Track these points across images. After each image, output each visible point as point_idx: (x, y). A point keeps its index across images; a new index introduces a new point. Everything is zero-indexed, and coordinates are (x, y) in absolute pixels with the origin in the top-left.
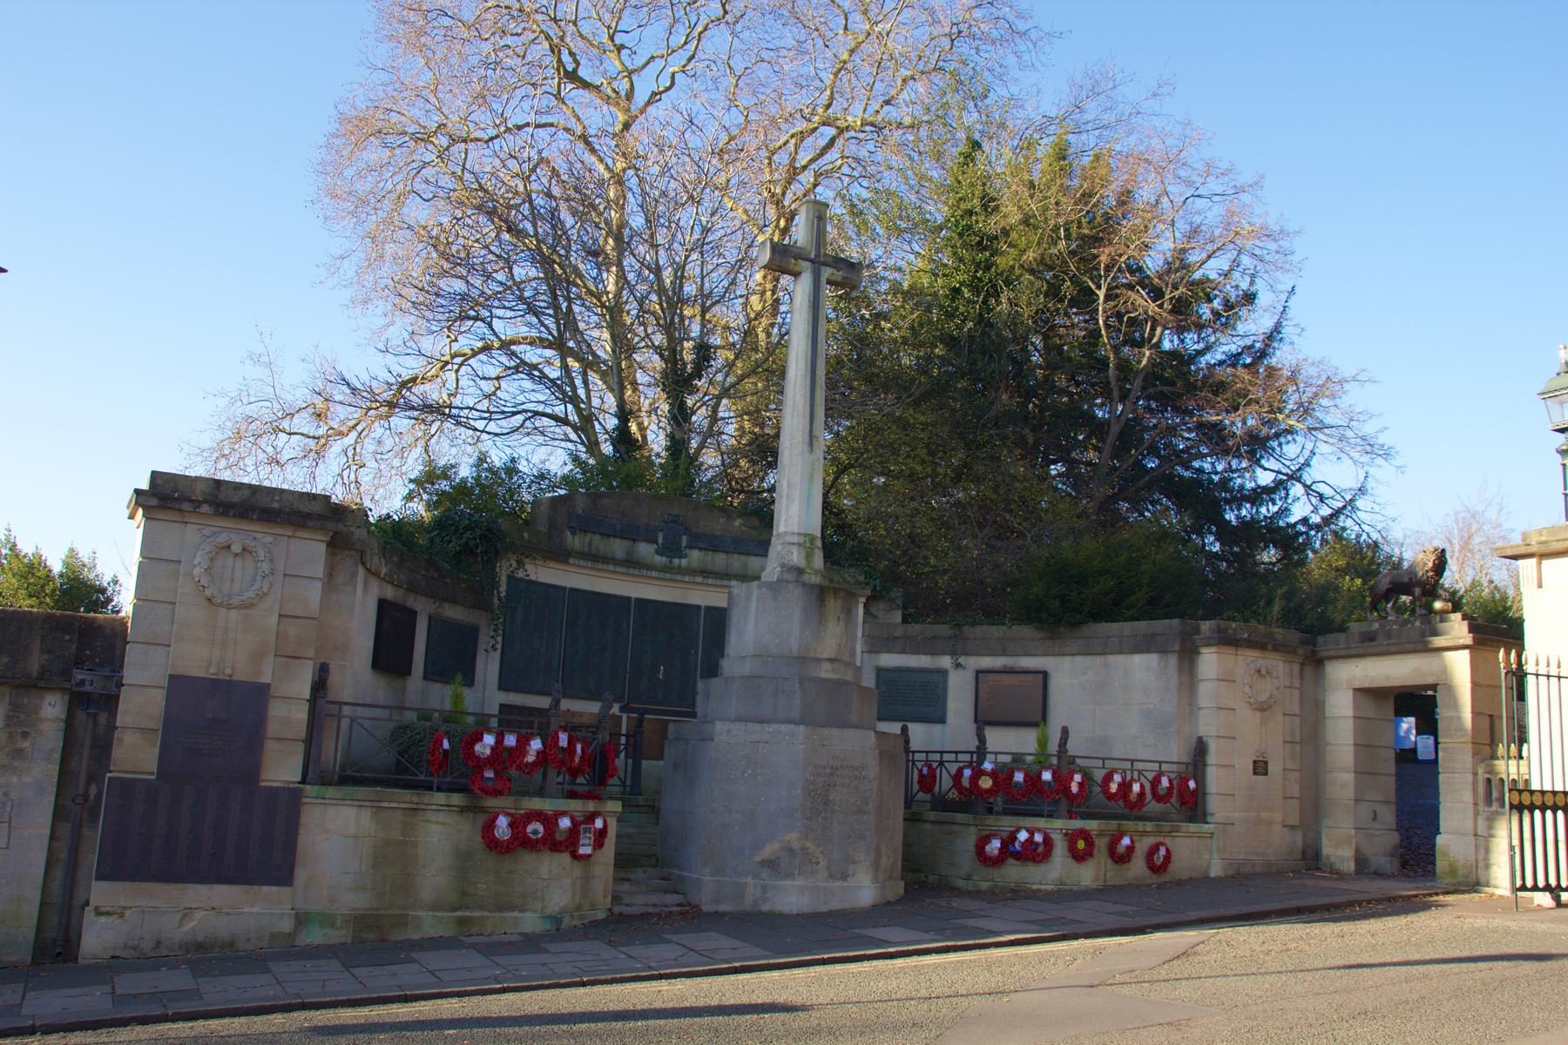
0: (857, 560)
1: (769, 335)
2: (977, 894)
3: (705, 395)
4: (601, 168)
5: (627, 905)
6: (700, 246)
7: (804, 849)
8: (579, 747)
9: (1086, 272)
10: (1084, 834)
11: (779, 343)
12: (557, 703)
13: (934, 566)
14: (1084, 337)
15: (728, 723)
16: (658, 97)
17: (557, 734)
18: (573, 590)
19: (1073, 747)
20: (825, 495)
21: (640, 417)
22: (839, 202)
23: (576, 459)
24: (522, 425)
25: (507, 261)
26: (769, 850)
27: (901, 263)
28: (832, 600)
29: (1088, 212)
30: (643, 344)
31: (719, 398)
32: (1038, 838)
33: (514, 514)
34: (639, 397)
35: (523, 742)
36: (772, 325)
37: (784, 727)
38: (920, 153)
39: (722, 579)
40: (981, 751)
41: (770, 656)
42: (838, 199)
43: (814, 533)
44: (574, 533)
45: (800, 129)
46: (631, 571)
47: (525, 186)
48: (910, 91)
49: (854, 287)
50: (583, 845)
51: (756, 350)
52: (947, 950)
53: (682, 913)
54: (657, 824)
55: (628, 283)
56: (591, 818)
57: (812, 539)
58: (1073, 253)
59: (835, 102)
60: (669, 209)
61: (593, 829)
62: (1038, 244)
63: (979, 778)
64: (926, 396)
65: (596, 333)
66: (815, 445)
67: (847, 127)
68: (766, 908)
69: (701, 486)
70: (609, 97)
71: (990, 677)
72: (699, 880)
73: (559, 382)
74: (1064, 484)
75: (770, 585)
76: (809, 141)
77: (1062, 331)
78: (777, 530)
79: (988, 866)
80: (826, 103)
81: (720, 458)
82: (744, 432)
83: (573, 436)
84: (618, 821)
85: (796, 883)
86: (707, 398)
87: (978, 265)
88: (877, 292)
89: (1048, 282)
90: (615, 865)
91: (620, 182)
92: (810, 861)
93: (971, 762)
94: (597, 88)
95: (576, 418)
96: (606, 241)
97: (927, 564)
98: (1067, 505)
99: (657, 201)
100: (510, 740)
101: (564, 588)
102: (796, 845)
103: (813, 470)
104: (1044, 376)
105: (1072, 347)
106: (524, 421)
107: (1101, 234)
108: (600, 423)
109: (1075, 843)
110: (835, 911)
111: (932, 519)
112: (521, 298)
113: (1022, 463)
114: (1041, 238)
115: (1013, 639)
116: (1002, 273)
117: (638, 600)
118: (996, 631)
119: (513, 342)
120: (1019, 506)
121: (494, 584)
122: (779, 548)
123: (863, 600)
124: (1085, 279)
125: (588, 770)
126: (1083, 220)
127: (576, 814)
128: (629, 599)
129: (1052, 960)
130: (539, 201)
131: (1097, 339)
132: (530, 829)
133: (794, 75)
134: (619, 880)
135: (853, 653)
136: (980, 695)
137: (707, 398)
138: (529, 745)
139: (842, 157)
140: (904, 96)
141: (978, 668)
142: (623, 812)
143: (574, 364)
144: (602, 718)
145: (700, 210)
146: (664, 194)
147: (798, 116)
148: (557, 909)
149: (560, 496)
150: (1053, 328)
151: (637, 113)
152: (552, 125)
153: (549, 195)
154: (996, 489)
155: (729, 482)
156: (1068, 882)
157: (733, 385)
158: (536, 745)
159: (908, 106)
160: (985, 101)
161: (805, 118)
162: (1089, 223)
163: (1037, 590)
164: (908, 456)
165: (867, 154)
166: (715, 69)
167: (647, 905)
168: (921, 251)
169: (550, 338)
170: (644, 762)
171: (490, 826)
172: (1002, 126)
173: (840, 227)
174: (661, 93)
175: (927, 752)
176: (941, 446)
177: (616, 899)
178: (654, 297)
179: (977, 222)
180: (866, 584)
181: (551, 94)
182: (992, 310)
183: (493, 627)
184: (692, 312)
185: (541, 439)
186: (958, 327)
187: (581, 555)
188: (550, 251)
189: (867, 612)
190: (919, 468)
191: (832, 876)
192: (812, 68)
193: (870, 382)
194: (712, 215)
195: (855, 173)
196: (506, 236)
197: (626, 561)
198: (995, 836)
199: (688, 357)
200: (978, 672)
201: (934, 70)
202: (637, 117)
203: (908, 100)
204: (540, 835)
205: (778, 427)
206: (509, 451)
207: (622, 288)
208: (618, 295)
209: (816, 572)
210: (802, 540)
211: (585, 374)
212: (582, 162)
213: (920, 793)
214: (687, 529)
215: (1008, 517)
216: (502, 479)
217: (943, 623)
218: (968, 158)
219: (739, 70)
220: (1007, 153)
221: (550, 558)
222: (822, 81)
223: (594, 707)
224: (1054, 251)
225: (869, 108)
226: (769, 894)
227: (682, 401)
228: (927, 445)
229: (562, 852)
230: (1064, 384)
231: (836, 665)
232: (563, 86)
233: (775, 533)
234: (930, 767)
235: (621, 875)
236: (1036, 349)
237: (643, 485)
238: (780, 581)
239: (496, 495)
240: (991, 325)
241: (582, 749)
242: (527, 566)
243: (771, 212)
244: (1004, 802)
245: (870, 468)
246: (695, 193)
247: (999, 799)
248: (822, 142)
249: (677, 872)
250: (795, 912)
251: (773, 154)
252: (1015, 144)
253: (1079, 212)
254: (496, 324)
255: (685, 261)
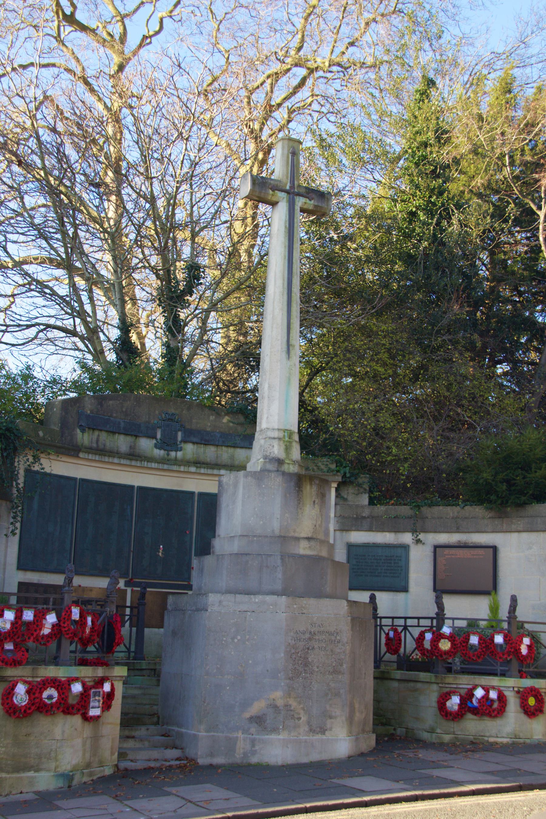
0: (330, 450)
1: (250, 255)
2: (440, 746)
3: (196, 309)
4: (101, 107)
5: (132, 761)
6: (189, 178)
7: (287, 706)
8: (89, 619)
9: (528, 194)
10: (534, 692)
11: (259, 263)
12: (69, 581)
13: (396, 456)
14: (526, 253)
15: (219, 595)
16: (148, 41)
17: (70, 609)
18: (83, 481)
19: (521, 614)
20: (301, 394)
21: (138, 327)
22: (309, 136)
23: (84, 366)
24: (36, 337)
25: (19, 190)
26: (256, 708)
27: (366, 193)
28: (308, 487)
29: (530, 141)
30: (140, 265)
31: (207, 312)
32: (493, 695)
33: (29, 414)
34: (138, 310)
35: (40, 617)
36: (253, 246)
37: (269, 599)
38: (381, 91)
39: (213, 468)
40: (440, 617)
41: (255, 536)
42: (309, 134)
43: (292, 429)
44: (83, 431)
45: (275, 71)
46: (134, 463)
47: (33, 124)
48: (372, 33)
49: (324, 215)
50: (93, 708)
51: (238, 268)
52: (415, 799)
53: (180, 767)
54: (158, 685)
55: (127, 212)
56: (100, 682)
57: (291, 434)
58: (517, 178)
59: (305, 44)
60: (161, 145)
61: (101, 693)
62: (486, 170)
63: (439, 641)
64: (388, 306)
65: (99, 255)
66: (292, 352)
67: (317, 68)
68: (254, 760)
69: (193, 389)
70: (105, 40)
71: (447, 551)
72: (195, 735)
73: (68, 299)
74: (509, 381)
75: (254, 474)
76: (283, 81)
77: (507, 248)
78: (260, 426)
79: (449, 719)
80: (297, 45)
81: (209, 362)
82: (229, 341)
83: (81, 345)
84: (124, 684)
85: (281, 737)
86: (197, 312)
87: (432, 191)
88: (344, 216)
89: (494, 205)
90: (121, 724)
91: (118, 120)
92: (293, 717)
93: (432, 627)
94: (93, 31)
95: (83, 328)
96: (106, 174)
97: (390, 454)
98: (512, 400)
99: (151, 139)
100: (28, 615)
101: (74, 479)
102: (280, 703)
103: (290, 374)
104: (490, 287)
105: (515, 262)
106: (38, 333)
107: (542, 161)
108: (104, 334)
109: (527, 700)
110: (315, 762)
111: (394, 414)
112: (32, 224)
113: (471, 363)
114: (488, 165)
115: (466, 518)
116: (453, 197)
117: (140, 488)
118: (451, 511)
119: (25, 262)
120: (469, 402)
121: (14, 477)
122: (262, 442)
123: (335, 485)
124: (527, 201)
125: (98, 639)
126: (526, 148)
127: (87, 680)
128: (133, 487)
129: (511, 810)
130: (46, 136)
131: (538, 254)
132: (45, 694)
133: (269, 19)
134: (124, 738)
135: (327, 533)
136: (438, 567)
137: (197, 312)
138: (45, 619)
139: (312, 95)
140: (367, 38)
141: (436, 543)
142: (128, 676)
143: (80, 282)
144: (109, 593)
145: (188, 145)
146: (156, 131)
147: (273, 58)
148: (69, 767)
149: (72, 399)
150: (497, 246)
151: (130, 55)
152: (54, 65)
153: (54, 130)
154: (449, 388)
155: (218, 384)
156: (521, 735)
157: (220, 300)
158: (51, 618)
159: (370, 47)
160: (440, 41)
161: (279, 60)
162: (531, 150)
163: (486, 475)
164: (372, 360)
165: (334, 93)
166: (199, 14)
167: (149, 760)
168: (381, 179)
169: (59, 258)
170: (147, 630)
171: (9, 693)
172: (455, 63)
173: (311, 159)
174: (151, 37)
175: (393, 618)
176: (401, 350)
177: (122, 755)
178: (149, 223)
179: (431, 153)
180: (338, 471)
181: (52, 36)
182: (444, 230)
183: (12, 515)
184: (183, 236)
185: (52, 348)
186: (414, 246)
187: (90, 450)
188: (57, 182)
189: (338, 496)
190: (381, 370)
191: (312, 731)
192: (285, 14)
193: (339, 296)
194: (199, 150)
195: (324, 110)
196: (16, 168)
197: (130, 455)
198: (454, 693)
199: (180, 276)
200: (436, 547)
201: (394, 12)
202: (130, 59)
203: (370, 42)
204: (54, 700)
205: (259, 335)
206: (24, 360)
207: (121, 216)
208: (118, 223)
209: (294, 462)
210: (281, 435)
211: (90, 291)
212: (83, 102)
213: (388, 655)
214: (182, 426)
215: (459, 410)
216: (19, 384)
217: (405, 505)
218: (424, 95)
219: (220, 16)
220: (459, 89)
221: (63, 454)
222: (294, 25)
223: (103, 583)
224: (499, 176)
225: (336, 49)
226: (257, 748)
227: (176, 314)
228: (389, 351)
229: (74, 714)
230: (508, 293)
231: (313, 543)
232: (62, 28)
233: (258, 429)
234: (395, 631)
235: (127, 733)
236: (483, 264)
237: (143, 388)
238: (263, 470)
239: (13, 399)
240: (443, 244)
241: (92, 621)
242: (43, 461)
243: (251, 146)
244: (462, 662)
245: (340, 370)
246: (183, 131)
247: (457, 660)
248: (295, 82)
249: (176, 729)
250: (280, 763)
251: (251, 94)
252: (466, 80)
253: (523, 141)
254: (10, 247)
255: (176, 192)
